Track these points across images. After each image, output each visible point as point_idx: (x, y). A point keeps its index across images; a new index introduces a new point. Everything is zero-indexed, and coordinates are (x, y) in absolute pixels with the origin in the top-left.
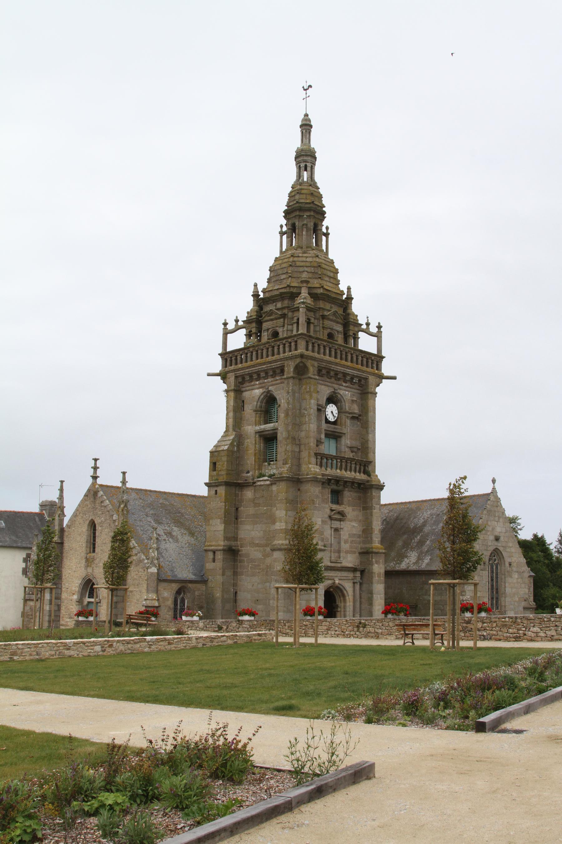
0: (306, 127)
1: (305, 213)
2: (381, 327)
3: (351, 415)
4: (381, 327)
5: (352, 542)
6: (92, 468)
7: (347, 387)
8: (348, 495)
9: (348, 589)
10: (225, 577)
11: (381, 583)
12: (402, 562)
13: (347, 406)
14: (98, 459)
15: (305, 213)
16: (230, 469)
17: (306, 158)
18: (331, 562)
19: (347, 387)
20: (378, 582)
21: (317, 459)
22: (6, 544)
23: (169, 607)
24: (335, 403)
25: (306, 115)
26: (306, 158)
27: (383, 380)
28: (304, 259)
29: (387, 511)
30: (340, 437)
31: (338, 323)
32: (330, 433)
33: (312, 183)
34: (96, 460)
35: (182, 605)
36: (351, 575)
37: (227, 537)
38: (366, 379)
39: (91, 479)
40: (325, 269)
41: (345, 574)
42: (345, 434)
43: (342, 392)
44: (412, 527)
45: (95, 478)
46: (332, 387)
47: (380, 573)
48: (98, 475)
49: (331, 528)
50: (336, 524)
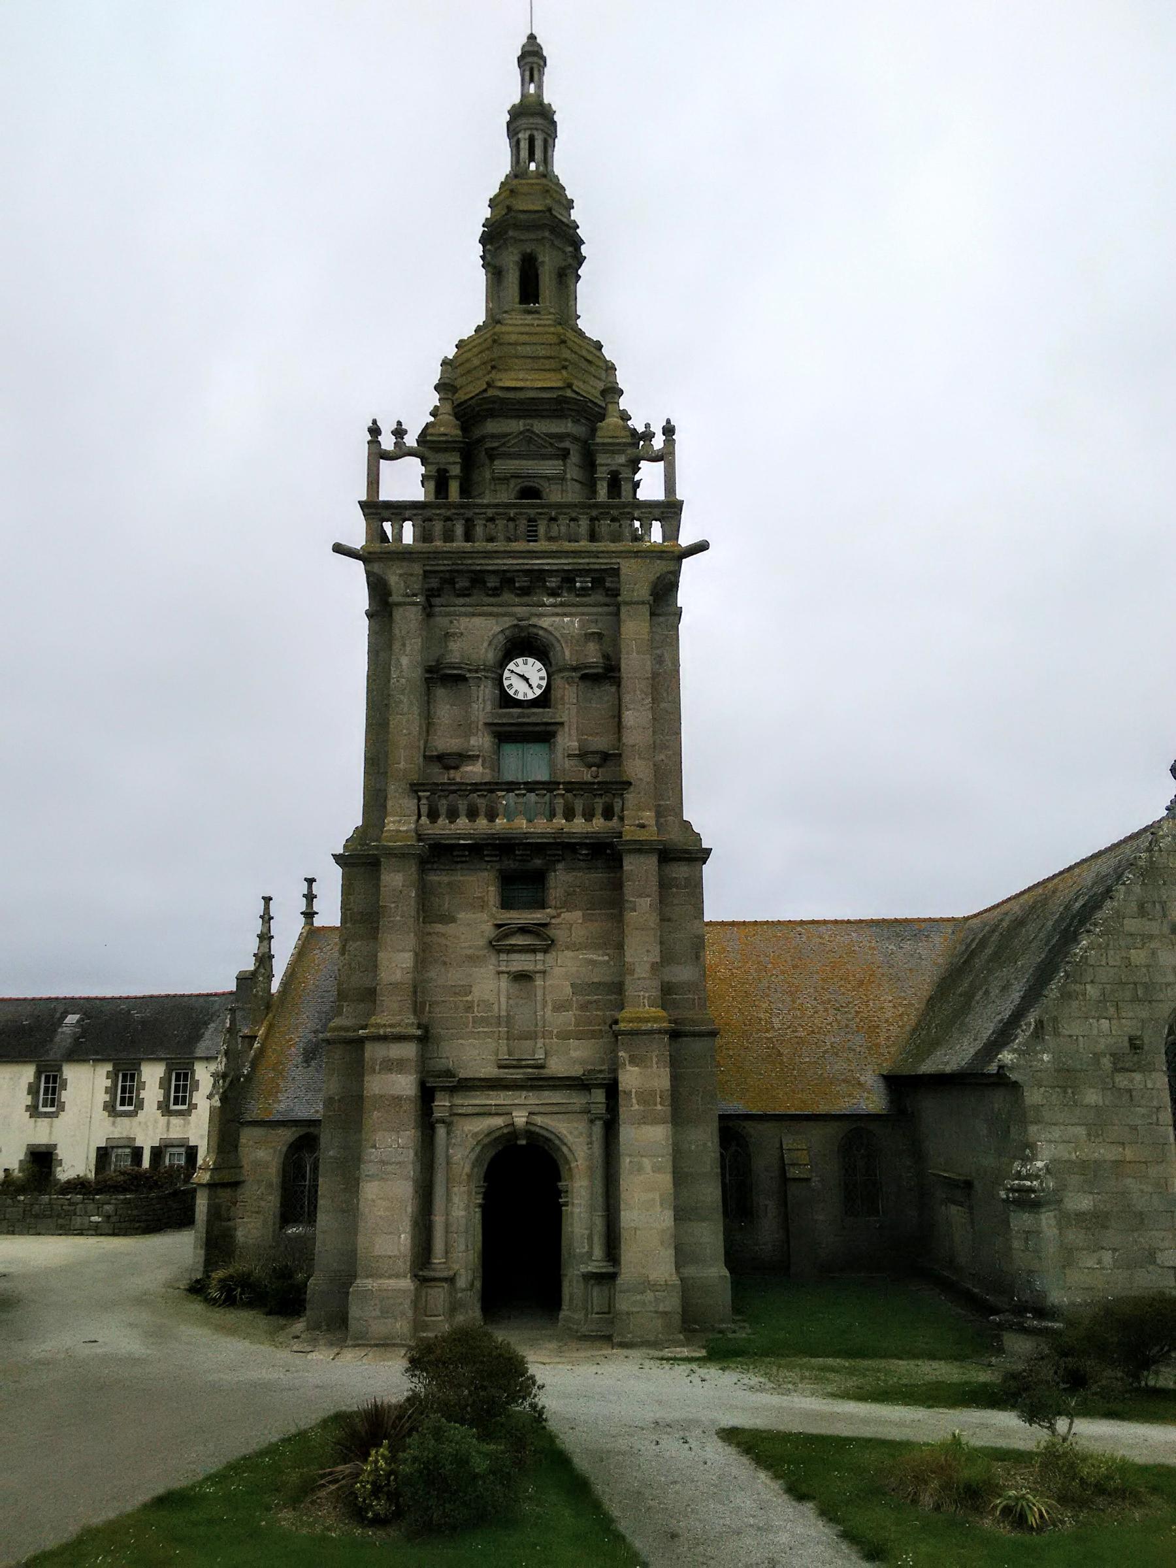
0: (532, 60)
1: (532, 241)
2: (405, 432)
3: (579, 675)
4: (405, 432)
5: (584, 1007)
6: (304, 896)
7: (562, 605)
8: (561, 880)
9: (570, 1139)
13: (566, 654)
14: (314, 880)
15: (532, 241)
17: (532, 124)
18: (500, 1067)
19: (562, 605)
20: (645, 1119)
21: (419, 799)
23: (270, 1185)
25: (532, 37)
26: (532, 124)
30: (553, 735)
33: (547, 175)
36: (577, 1100)
38: (616, 572)
39: (302, 919)
41: (556, 1097)
42: (562, 724)
43: (545, 622)
45: (309, 915)
50: (520, 962)
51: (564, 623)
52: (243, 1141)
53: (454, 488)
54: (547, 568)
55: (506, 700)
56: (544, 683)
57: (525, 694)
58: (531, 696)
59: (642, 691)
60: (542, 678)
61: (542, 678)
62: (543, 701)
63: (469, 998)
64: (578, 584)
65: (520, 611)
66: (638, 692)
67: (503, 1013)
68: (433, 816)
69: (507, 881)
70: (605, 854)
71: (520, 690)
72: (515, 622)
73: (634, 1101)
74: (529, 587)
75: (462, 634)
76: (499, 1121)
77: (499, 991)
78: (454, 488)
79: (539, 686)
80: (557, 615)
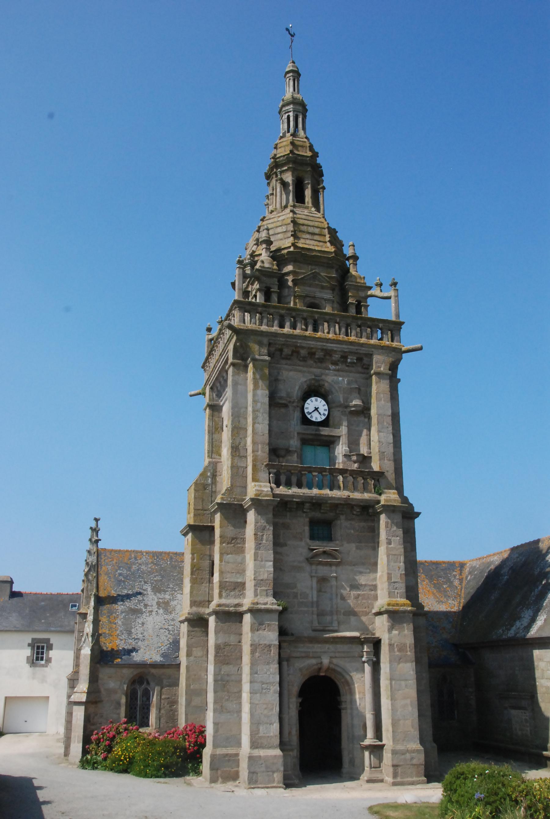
10: (192, 658)
11: (406, 662)
12: (512, 626)
16: (200, 507)
21: (270, 474)
22: (18, 629)
24: (324, 397)
27: (403, 355)
28: (276, 220)
29: (517, 555)
31: (323, 287)
32: (310, 437)
34: (97, 520)
35: (145, 699)
37: (195, 602)
40: (303, 225)
42: (339, 437)
44: (536, 573)
46: (309, 372)
47: (405, 645)
48: (100, 537)
49: (312, 577)
50: (323, 571)
51: (337, 379)
52: (101, 676)
53: (275, 297)
54: (335, 349)
55: (305, 421)
56: (326, 413)
57: (316, 418)
58: (319, 420)
59: (387, 423)
60: (325, 410)
61: (325, 410)
62: (325, 423)
63: (295, 590)
64: (349, 360)
65: (317, 371)
66: (385, 424)
67: (315, 599)
68: (278, 484)
69: (313, 523)
70: (368, 512)
71: (316, 417)
72: (313, 377)
73: (396, 650)
74: (323, 359)
75: (285, 380)
76: (314, 661)
77: (312, 588)
78: (275, 297)
79: (324, 414)
80: (336, 375)
